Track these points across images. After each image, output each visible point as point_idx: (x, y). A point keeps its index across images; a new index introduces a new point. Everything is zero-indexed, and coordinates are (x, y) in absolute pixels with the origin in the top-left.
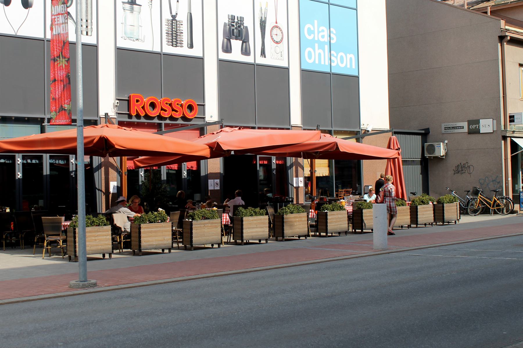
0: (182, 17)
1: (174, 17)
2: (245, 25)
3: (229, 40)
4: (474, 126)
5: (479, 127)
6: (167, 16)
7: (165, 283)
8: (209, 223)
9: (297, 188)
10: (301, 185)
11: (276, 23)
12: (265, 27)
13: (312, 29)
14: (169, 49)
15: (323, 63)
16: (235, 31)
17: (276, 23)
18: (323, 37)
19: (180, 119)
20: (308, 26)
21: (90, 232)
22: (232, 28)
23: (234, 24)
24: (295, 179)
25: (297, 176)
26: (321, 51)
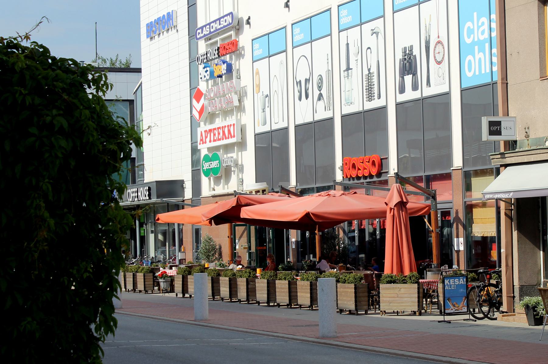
0: (374, 70)
1: (370, 73)
2: (414, 54)
3: (403, 78)
4: (496, 128)
5: (500, 129)
6: (366, 72)
7: (255, 333)
8: (405, 288)
9: (458, 252)
10: (462, 248)
11: (438, 37)
12: (429, 47)
13: (472, 27)
14: (369, 106)
15: (483, 72)
16: (408, 66)
17: (438, 37)
18: (483, 32)
19: (375, 176)
20: (469, 24)
21: (259, 283)
22: (406, 62)
23: (406, 57)
24: (455, 239)
25: (458, 237)
26: (481, 55)
